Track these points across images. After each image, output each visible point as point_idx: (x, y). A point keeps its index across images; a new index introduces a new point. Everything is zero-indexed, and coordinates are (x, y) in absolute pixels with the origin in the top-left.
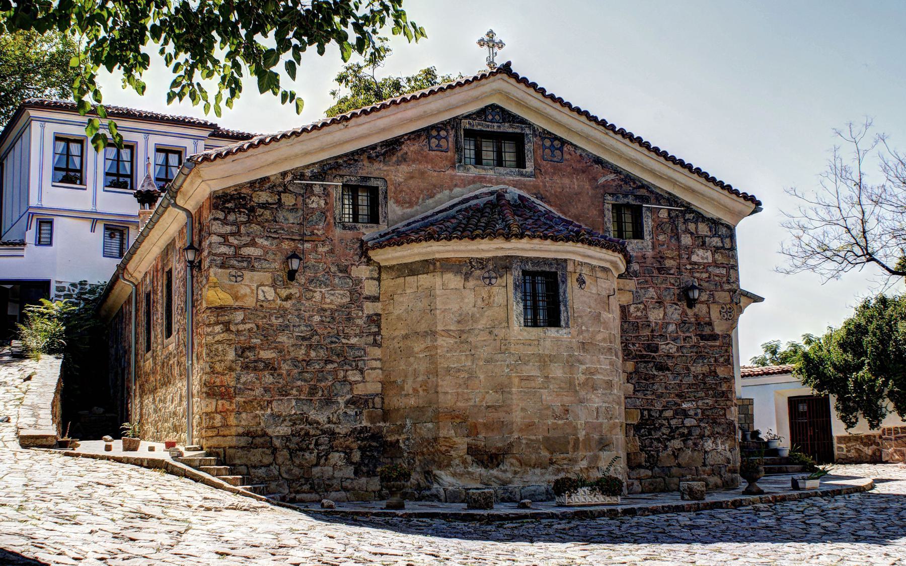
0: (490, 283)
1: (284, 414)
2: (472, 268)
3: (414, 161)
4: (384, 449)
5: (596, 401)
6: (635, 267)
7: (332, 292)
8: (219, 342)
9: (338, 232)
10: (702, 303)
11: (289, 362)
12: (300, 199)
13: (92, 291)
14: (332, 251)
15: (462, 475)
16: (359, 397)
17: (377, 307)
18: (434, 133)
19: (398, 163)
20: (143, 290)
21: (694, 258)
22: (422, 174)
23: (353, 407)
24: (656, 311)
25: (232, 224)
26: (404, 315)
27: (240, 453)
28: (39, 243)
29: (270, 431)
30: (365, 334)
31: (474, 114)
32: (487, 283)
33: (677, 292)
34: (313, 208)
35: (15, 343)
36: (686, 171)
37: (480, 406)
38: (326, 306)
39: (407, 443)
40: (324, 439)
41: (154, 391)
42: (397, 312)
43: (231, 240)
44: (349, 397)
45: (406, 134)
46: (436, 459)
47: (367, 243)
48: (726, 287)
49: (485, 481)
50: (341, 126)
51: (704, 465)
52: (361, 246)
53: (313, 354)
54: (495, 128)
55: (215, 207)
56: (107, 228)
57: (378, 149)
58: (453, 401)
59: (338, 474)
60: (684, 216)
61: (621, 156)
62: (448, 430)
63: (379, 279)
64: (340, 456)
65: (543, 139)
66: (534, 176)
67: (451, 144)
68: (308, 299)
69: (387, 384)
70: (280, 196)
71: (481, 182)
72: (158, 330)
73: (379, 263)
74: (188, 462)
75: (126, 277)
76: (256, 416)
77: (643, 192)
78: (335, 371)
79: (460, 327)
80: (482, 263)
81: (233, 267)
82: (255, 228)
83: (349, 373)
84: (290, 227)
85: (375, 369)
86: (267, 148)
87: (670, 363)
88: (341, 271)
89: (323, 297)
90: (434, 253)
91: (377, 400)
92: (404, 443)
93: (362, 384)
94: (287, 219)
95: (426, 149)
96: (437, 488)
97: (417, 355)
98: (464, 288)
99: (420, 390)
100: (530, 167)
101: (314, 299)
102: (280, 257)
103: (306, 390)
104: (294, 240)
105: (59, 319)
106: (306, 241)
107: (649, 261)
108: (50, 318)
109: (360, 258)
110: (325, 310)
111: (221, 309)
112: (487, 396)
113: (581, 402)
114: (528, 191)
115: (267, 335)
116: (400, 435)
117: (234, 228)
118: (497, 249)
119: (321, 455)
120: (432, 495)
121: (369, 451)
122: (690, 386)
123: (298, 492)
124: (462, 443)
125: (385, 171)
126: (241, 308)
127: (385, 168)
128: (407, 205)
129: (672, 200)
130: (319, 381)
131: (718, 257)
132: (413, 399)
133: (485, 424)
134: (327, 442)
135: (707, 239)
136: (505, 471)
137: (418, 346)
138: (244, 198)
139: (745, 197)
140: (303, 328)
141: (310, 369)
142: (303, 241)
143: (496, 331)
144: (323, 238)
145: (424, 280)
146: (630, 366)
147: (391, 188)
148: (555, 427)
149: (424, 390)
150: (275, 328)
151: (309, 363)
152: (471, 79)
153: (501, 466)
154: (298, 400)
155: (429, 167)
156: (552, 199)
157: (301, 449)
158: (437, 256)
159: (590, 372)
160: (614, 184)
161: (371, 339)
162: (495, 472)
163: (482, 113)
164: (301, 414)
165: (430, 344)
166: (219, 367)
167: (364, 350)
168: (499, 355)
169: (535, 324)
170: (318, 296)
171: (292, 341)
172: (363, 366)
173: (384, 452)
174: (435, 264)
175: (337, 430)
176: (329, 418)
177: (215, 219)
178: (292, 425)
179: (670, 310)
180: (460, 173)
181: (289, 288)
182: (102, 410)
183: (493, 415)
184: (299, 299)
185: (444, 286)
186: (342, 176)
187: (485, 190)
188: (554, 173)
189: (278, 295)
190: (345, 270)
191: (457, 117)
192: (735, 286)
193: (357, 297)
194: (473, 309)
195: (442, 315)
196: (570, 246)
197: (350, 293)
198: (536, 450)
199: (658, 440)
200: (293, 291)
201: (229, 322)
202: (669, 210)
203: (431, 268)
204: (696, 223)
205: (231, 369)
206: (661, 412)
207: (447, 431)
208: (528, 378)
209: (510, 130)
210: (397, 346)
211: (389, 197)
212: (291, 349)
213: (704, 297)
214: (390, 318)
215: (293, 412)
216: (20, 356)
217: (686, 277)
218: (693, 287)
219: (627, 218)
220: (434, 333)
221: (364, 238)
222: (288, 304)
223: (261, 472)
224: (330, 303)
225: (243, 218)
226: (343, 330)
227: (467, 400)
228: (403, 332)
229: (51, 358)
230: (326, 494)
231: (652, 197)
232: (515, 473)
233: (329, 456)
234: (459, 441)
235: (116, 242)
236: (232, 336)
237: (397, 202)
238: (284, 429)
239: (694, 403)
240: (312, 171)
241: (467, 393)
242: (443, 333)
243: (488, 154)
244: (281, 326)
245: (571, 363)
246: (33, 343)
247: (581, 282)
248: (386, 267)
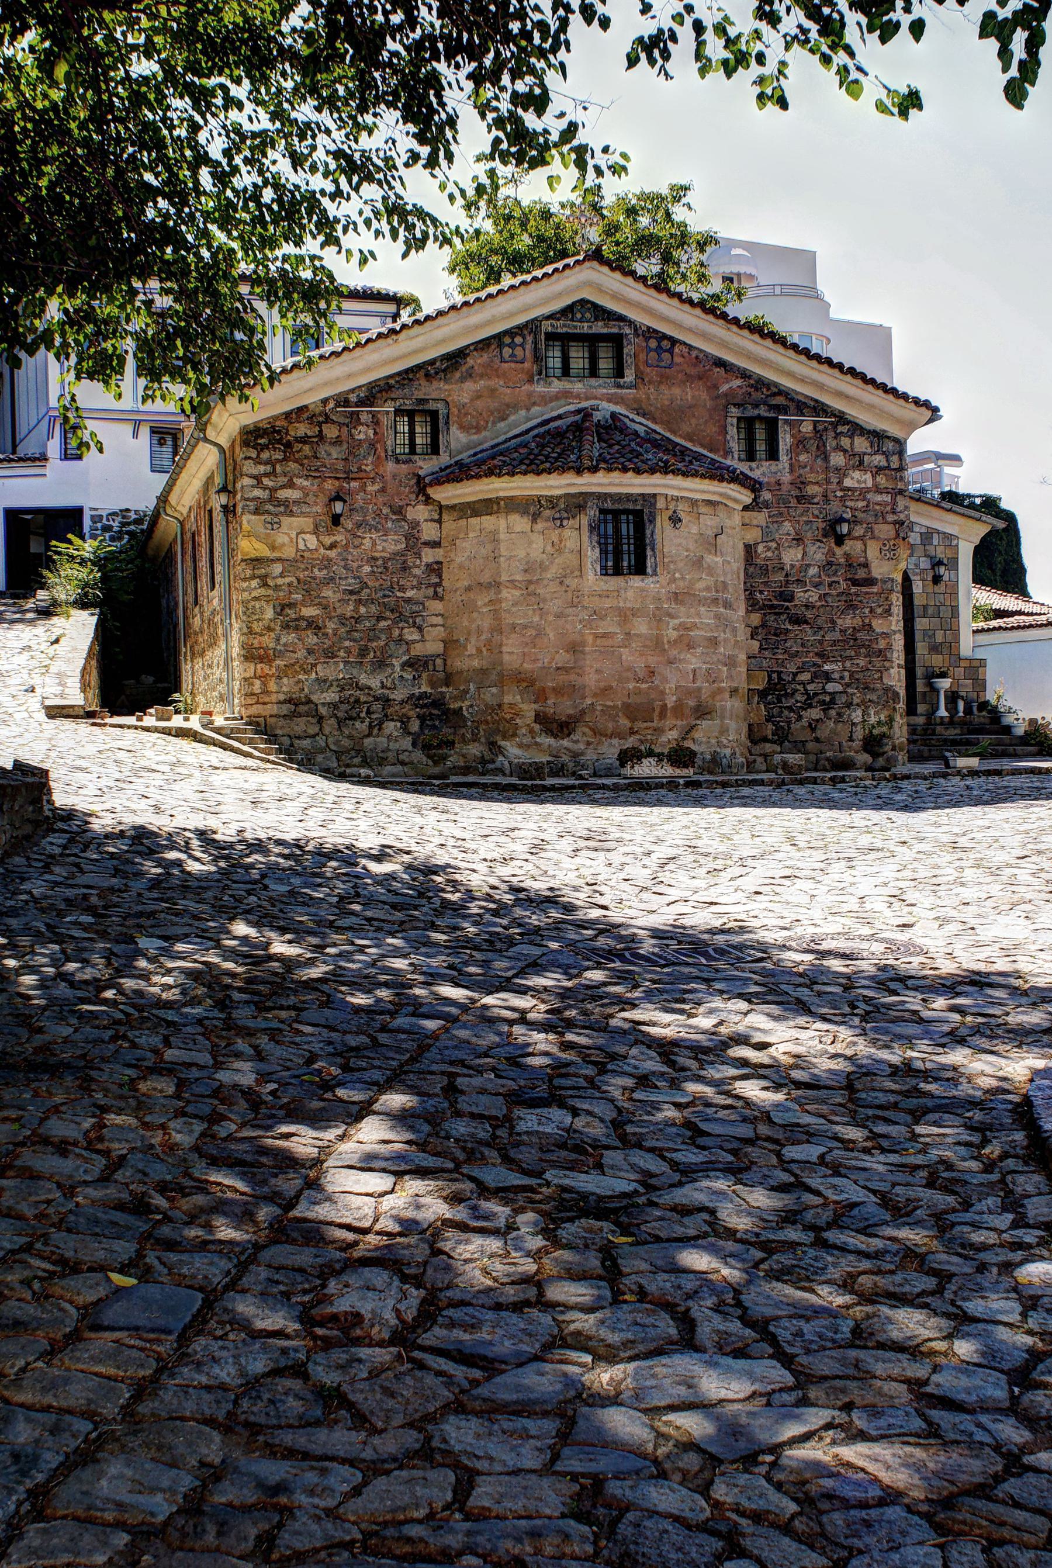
3: (482, 376)
5: (693, 661)
6: (766, 495)
8: (256, 599)
9: (390, 466)
10: (856, 538)
13: (138, 521)
14: (383, 490)
15: (528, 746)
16: (417, 659)
17: (438, 554)
18: (507, 340)
19: (463, 379)
20: (190, 526)
21: (848, 483)
22: (493, 391)
24: (792, 551)
25: (266, 463)
27: (281, 722)
28: (66, 456)
29: (314, 698)
33: (822, 525)
35: (41, 594)
36: (836, 372)
40: (377, 706)
41: (202, 654)
42: (458, 560)
43: (266, 481)
44: (405, 658)
48: (891, 518)
50: (389, 341)
52: (418, 483)
53: (363, 610)
54: (585, 328)
55: (246, 444)
56: (154, 431)
60: (835, 427)
63: (439, 522)
65: (647, 339)
66: (635, 387)
67: (529, 353)
69: (450, 643)
72: (204, 580)
74: (218, 731)
75: (169, 511)
76: (299, 681)
77: (780, 400)
78: (389, 629)
79: (528, 577)
80: (552, 502)
81: (269, 513)
82: (293, 466)
87: (809, 615)
89: (374, 544)
90: (497, 490)
91: (439, 661)
95: (497, 360)
100: (629, 376)
102: (323, 499)
103: (355, 651)
105: (94, 564)
107: (785, 488)
108: (83, 562)
110: (375, 559)
111: (256, 562)
113: (670, 662)
114: (628, 407)
115: (309, 589)
117: (269, 468)
122: (835, 643)
123: (348, 766)
124: (529, 710)
126: (279, 559)
129: (819, 408)
131: (881, 480)
136: (577, 742)
137: (482, 599)
138: (279, 432)
139: (917, 402)
142: (348, 479)
143: (567, 581)
145: (488, 522)
146: (756, 619)
147: (455, 411)
148: (638, 692)
151: (358, 620)
154: (346, 663)
156: (657, 415)
157: (351, 718)
158: (502, 494)
159: (685, 627)
161: (430, 591)
162: (565, 743)
163: (568, 311)
166: (257, 627)
169: (617, 572)
170: (367, 543)
171: (339, 596)
173: (447, 721)
177: (247, 458)
179: (811, 549)
180: (540, 388)
182: (151, 679)
183: (563, 678)
185: (509, 530)
187: (572, 408)
190: (399, 512)
192: (902, 517)
193: (413, 542)
196: (657, 479)
198: (614, 718)
199: (790, 709)
200: (338, 538)
201: (266, 576)
202: (815, 423)
204: (851, 437)
205: (269, 629)
206: (795, 675)
207: (512, 697)
208: (605, 636)
209: (605, 331)
213: (859, 531)
216: (46, 612)
217: (835, 508)
218: (841, 520)
219: (760, 434)
220: (497, 585)
221: (422, 473)
222: (332, 554)
223: (306, 743)
225: (279, 456)
227: (535, 661)
229: (84, 614)
231: (792, 406)
232: (588, 743)
235: (168, 449)
236: (270, 592)
237: (462, 428)
238: (331, 696)
243: (579, 359)
245: (658, 618)
246: (61, 594)
247: (675, 520)
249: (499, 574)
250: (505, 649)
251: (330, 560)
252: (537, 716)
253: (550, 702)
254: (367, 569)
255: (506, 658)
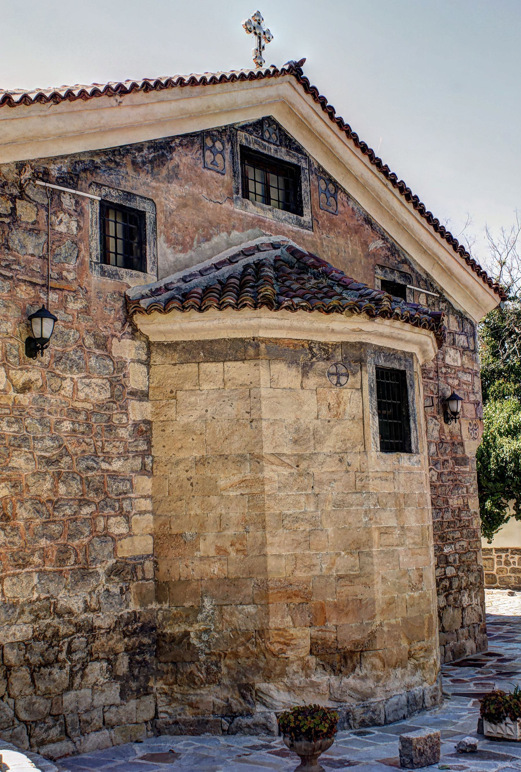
0: (338, 383)
1: (21, 600)
2: (313, 356)
3: (187, 180)
4: (159, 647)
7: (87, 381)
11: (28, 504)
12: (43, 213)
14: (86, 310)
18: (209, 142)
19: (169, 179)
23: (117, 579)
26: (199, 426)
30: (131, 455)
31: (250, 125)
32: (335, 382)
34: (61, 233)
37: (329, 577)
38: (79, 405)
39: (205, 637)
40: (79, 642)
42: (183, 420)
44: (111, 562)
45: (178, 137)
46: (262, 664)
47: (138, 301)
49: (337, 696)
50: (112, 101)
51: (462, 627)
53: (62, 489)
57: (145, 151)
58: (290, 569)
59: (100, 700)
61: (393, 217)
62: (283, 617)
64: (101, 669)
68: (55, 392)
70: (14, 202)
71: (260, 227)
73: (147, 337)
78: (92, 519)
83: (112, 520)
84: (28, 262)
85: (144, 512)
86: (13, 112)
88: (98, 347)
89: (75, 390)
91: (149, 565)
92: (200, 638)
93: (129, 538)
94: (23, 247)
96: (263, 713)
97: (225, 493)
98: (302, 388)
99: (230, 549)
101: (63, 392)
102: (14, 313)
103: (53, 555)
104: (34, 284)
106: (54, 289)
109: (123, 325)
110: (76, 411)
112: (338, 561)
116: (191, 625)
118: (354, 330)
119: (75, 669)
120: (255, 725)
121: (139, 654)
125: (154, 188)
127: (154, 184)
128: (180, 248)
130: (71, 536)
132: (217, 565)
133: (336, 606)
134: (83, 646)
135: (457, 336)
140: (49, 443)
141: (58, 515)
142: (47, 288)
144: (75, 287)
147: (160, 216)
149: (238, 551)
150: (6, 442)
152: (48, 95)
153: (357, 670)
154: (42, 573)
155: (205, 193)
157: (48, 664)
158: (262, 334)
160: (383, 253)
162: (351, 681)
164: (47, 599)
165: (249, 476)
167: (130, 481)
168: (354, 496)
170: (67, 384)
171: (31, 466)
172: (129, 509)
174: (258, 346)
175: (98, 623)
176: (85, 602)
178: (34, 621)
181: (28, 370)
184: (42, 389)
186: (99, 186)
187: (264, 239)
188: (330, 229)
189: (11, 381)
191: (232, 126)
194: (316, 422)
195: (270, 430)
197: (111, 385)
203: (251, 351)
209: (287, 159)
210: (184, 475)
211: (158, 231)
212: (31, 480)
214: (169, 430)
215: (36, 596)
221: (131, 294)
222: (25, 399)
224: (85, 400)
226: (103, 448)
227: (311, 567)
228: (197, 454)
230: (82, 738)
232: (378, 679)
233: (87, 670)
234: (299, 634)
237: (170, 241)
239: (453, 546)
240: (60, 169)
241: (309, 556)
242: (272, 459)
244: (15, 438)
248: (160, 345)
249: (259, 443)
250: (270, 550)
251: (22, 409)
252: (314, 644)
253: (330, 625)
254: (67, 426)
255: (272, 563)
